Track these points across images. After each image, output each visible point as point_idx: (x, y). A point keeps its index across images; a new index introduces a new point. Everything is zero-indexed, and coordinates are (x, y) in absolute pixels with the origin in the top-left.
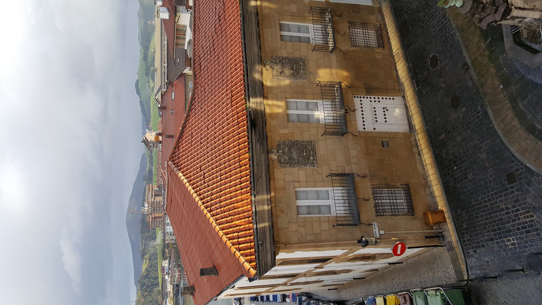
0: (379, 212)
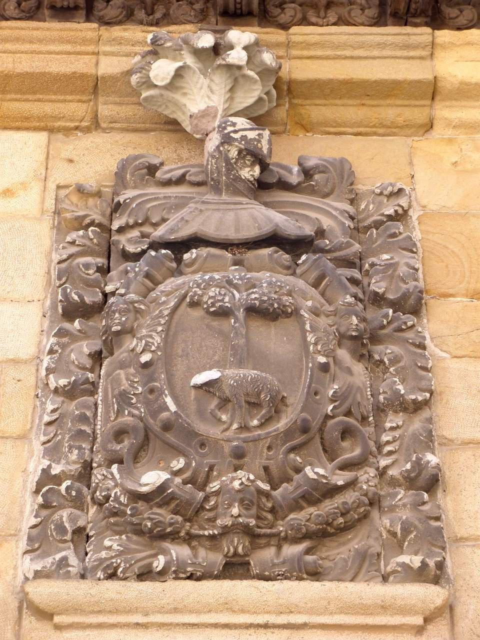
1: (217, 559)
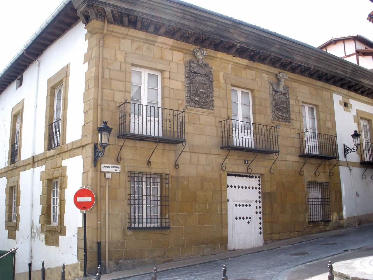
0: (133, 176)
1: (199, 106)
